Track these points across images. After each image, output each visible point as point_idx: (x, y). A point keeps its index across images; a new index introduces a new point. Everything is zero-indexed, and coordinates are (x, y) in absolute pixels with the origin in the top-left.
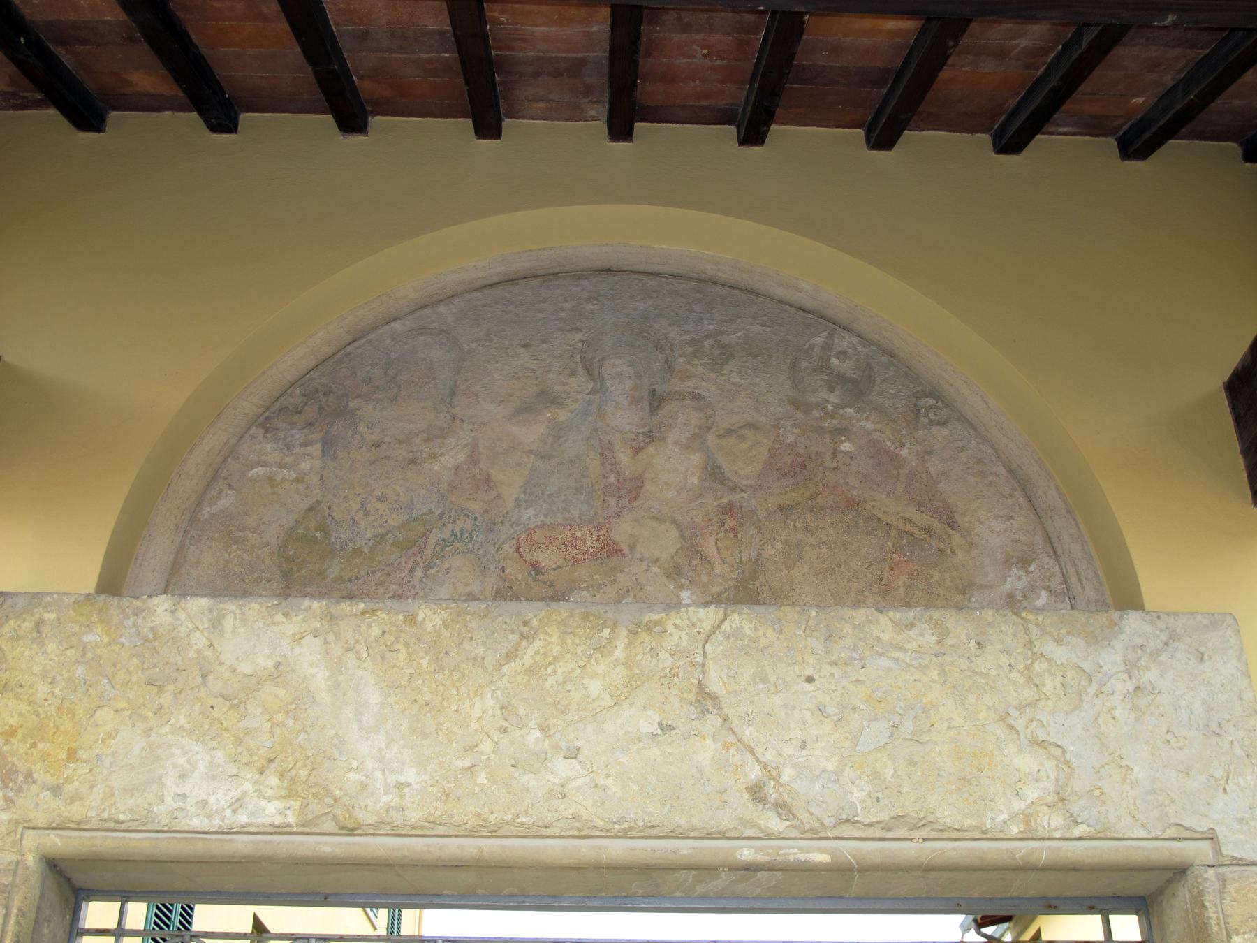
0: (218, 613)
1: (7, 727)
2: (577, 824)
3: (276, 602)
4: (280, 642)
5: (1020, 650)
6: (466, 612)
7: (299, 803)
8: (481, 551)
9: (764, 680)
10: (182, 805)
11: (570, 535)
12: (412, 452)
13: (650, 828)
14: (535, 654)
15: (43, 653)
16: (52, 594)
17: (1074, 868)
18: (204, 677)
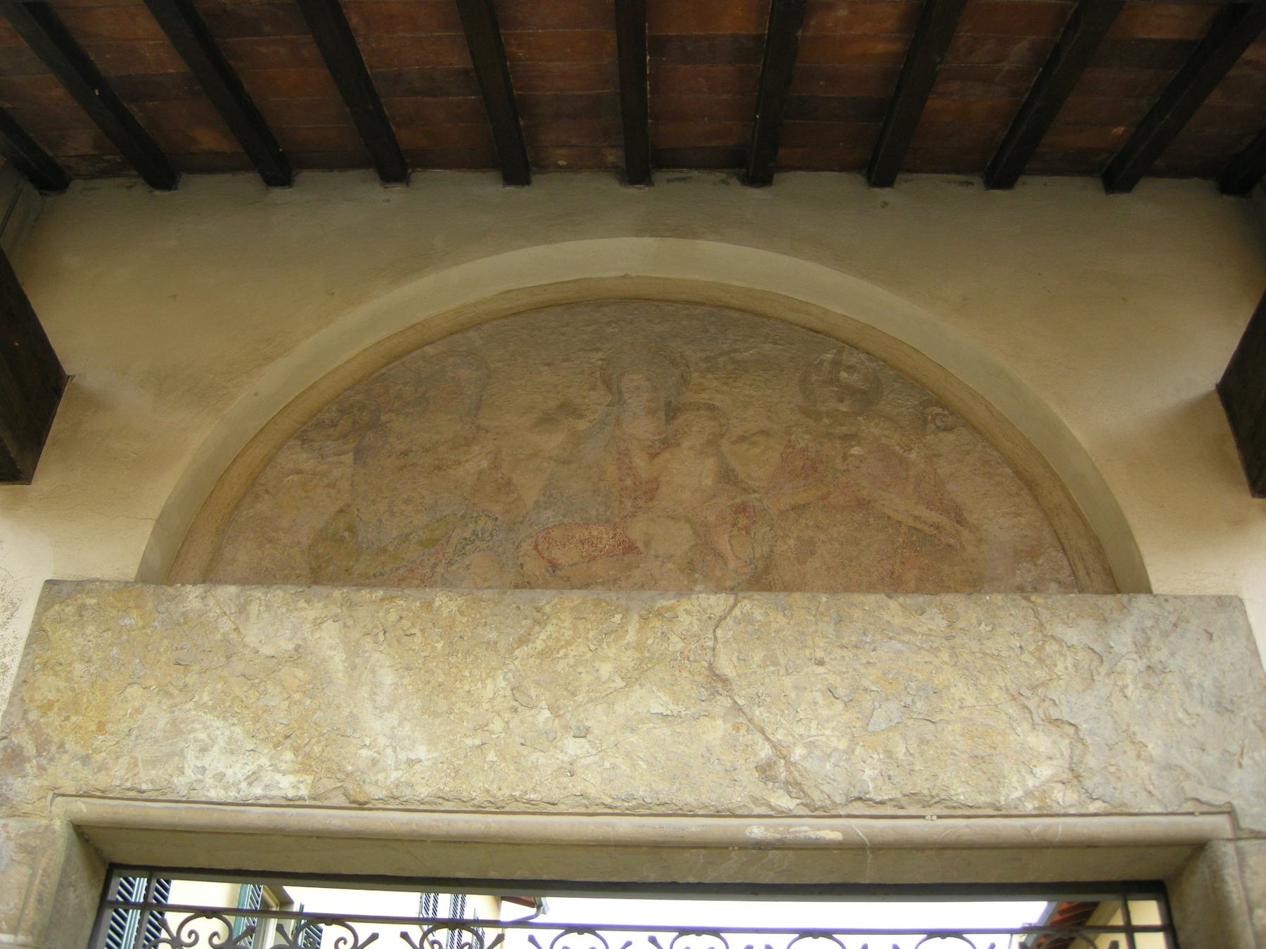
0: (244, 600)
1: (45, 701)
3: (300, 590)
4: (301, 627)
5: (1031, 632)
6: (481, 600)
7: (312, 777)
8: (501, 549)
9: (775, 663)
10: (200, 777)
11: (587, 534)
12: (438, 459)
13: (658, 805)
14: (547, 638)
15: (83, 635)
17: (1091, 846)
18: (228, 658)
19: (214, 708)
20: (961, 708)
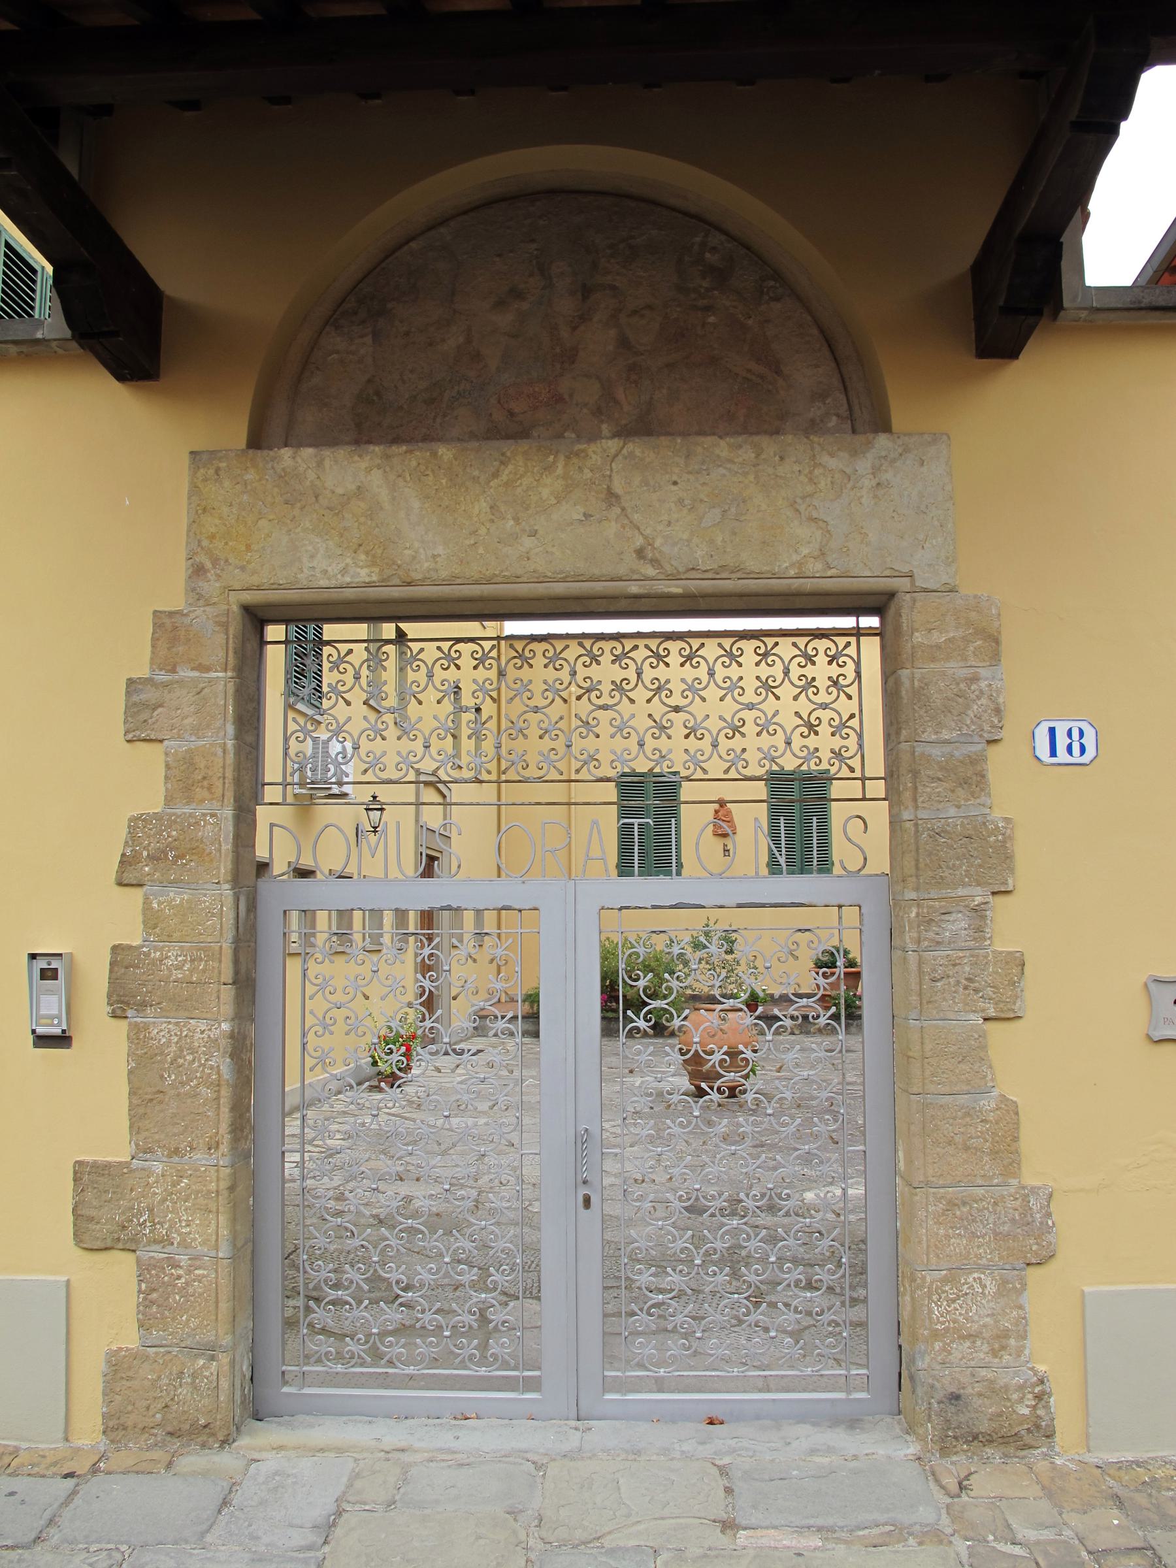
2: (536, 575)
9: (647, 484)
16: (221, 451)
18: (316, 497)
19: (313, 530)
20: (758, 511)
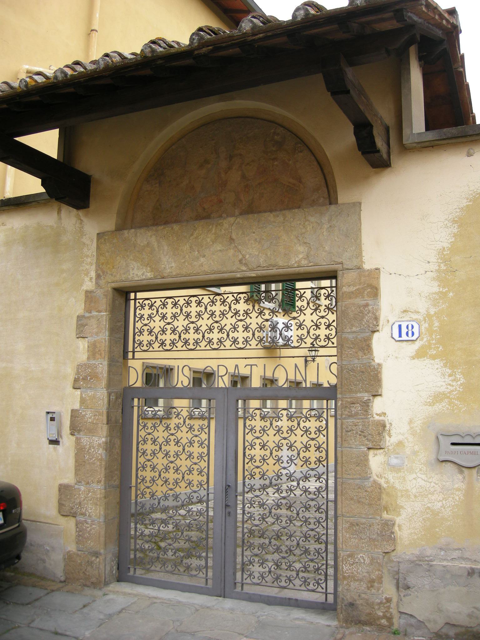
9: (244, 234)
18: (135, 247)
